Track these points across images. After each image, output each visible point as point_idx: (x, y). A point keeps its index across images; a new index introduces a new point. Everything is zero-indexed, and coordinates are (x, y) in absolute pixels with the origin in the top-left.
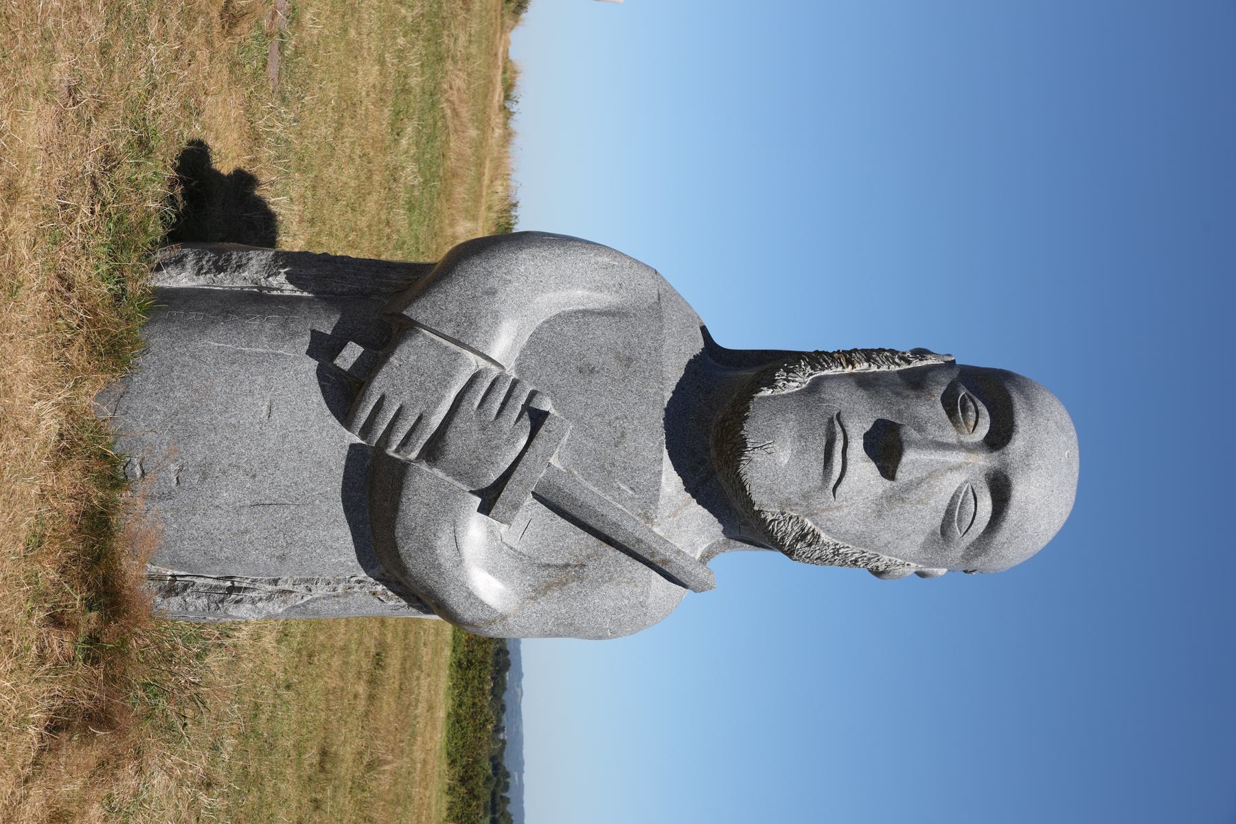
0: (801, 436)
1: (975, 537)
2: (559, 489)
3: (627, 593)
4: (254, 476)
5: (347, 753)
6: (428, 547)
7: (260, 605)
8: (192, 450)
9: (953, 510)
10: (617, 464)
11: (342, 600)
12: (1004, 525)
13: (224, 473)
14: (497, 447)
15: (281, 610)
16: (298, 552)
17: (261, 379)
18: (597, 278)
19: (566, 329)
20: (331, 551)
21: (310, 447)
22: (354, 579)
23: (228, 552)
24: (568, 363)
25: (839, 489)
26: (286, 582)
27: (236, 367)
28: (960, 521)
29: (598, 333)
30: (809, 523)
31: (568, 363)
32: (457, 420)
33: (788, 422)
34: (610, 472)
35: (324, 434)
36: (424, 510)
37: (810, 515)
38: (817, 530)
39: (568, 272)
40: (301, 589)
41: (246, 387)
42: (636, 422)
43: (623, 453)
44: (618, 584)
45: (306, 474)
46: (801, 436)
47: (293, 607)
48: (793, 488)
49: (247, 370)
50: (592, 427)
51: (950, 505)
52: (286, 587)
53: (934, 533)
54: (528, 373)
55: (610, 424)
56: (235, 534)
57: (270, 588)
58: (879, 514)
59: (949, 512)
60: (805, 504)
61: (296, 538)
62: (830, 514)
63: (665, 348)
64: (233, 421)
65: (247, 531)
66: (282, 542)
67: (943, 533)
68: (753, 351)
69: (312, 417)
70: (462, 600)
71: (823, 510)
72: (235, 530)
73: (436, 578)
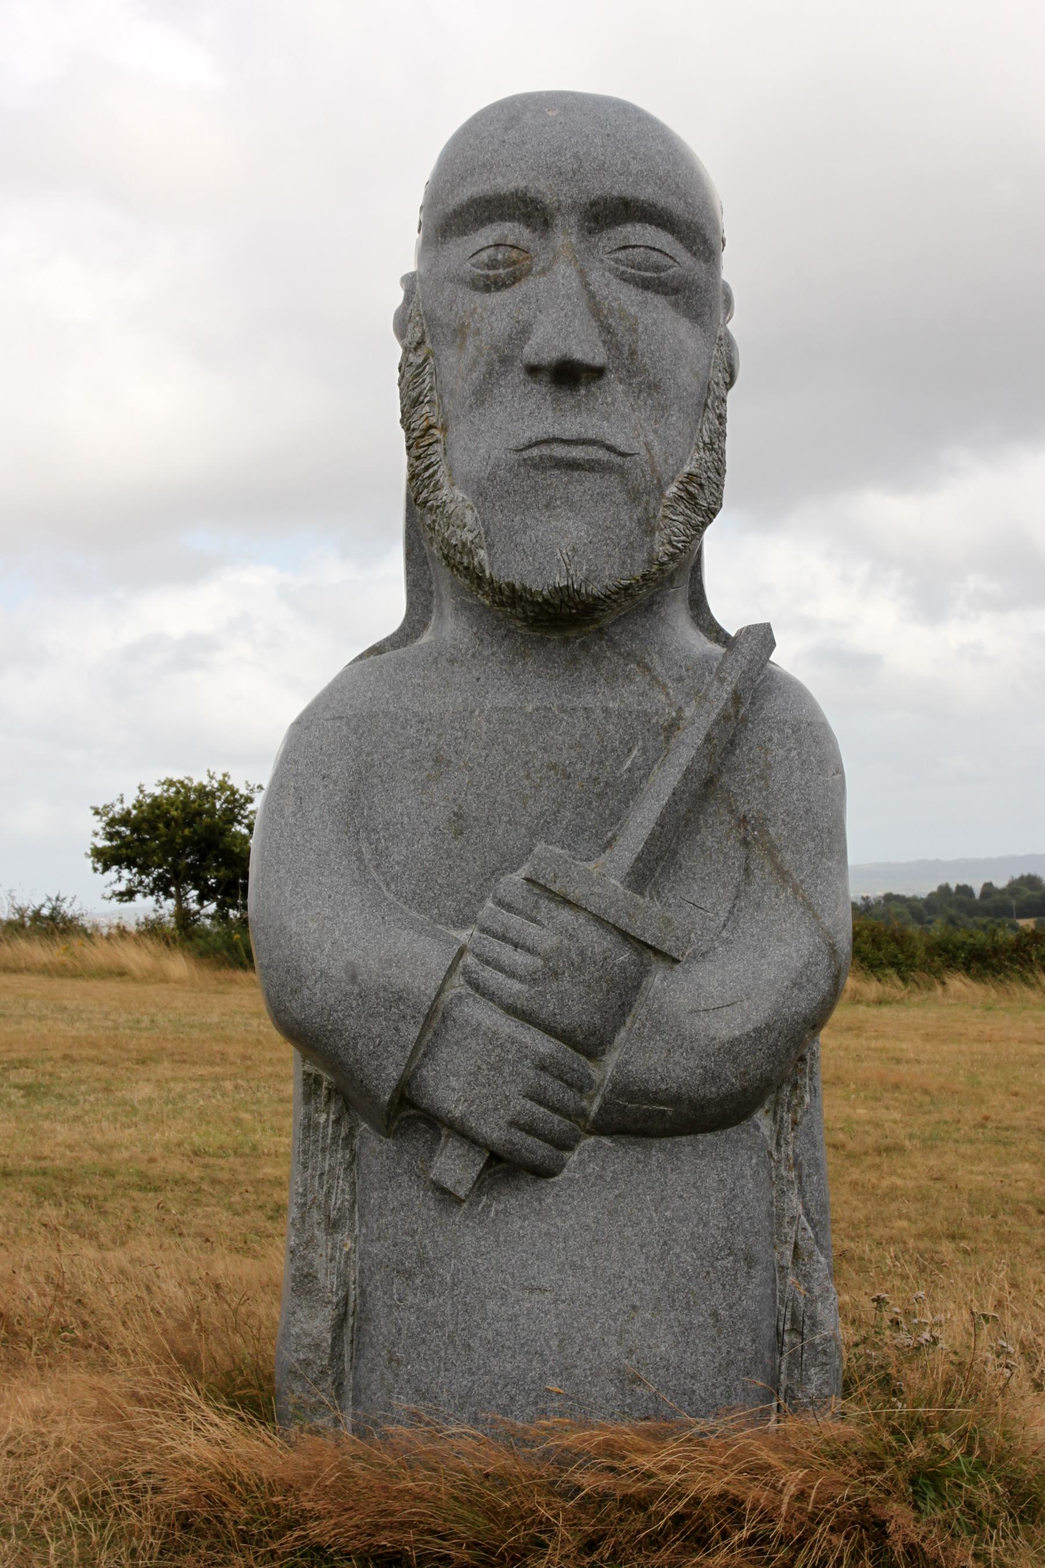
0: (547, 506)
1: (679, 246)
2: (639, 859)
3: (781, 752)
4: (634, 1307)
5: (269, 1070)
6: (730, 1049)
7: (817, 1291)
8: (600, 1401)
9: (644, 280)
10: (595, 774)
11: (806, 1171)
12: (661, 203)
13: (631, 1352)
14: (582, 953)
15: (822, 1259)
16: (741, 1238)
17: (491, 1305)
18: (317, 812)
19: (397, 857)
20: (738, 1191)
21: (587, 1228)
22: (775, 1153)
23: (745, 1341)
24: (448, 852)
25: (623, 448)
26: (782, 1254)
27: (475, 1343)
28: (657, 268)
29: (399, 808)
30: (672, 490)
31: (448, 852)
32: (544, 1014)
33: (527, 526)
34: (607, 783)
35: (568, 1208)
36: (677, 1057)
37: (661, 488)
38: (681, 477)
39: (312, 856)
40: (790, 1231)
41: (504, 1327)
42: (532, 749)
43: (579, 766)
44: (769, 766)
45: (628, 1232)
46: (547, 506)
47: (817, 1242)
48: (624, 516)
49: (478, 1326)
50: (543, 814)
51: (636, 284)
52: (789, 1254)
53: (675, 305)
54: (467, 910)
55: (537, 787)
56: (720, 1332)
57: (791, 1279)
58: (654, 387)
59: (646, 285)
60: (645, 498)
61: (722, 1242)
62: (659, 459)
63: (417, 708)
64: (554, 1343)
65: (715, 1314)
66: (728, 1262)
67: (676, 291)
68: (408, 573)
69: (544, 1228)
70: (804, 995)
71: (654, 471)
72: (714, 1332)
73: (775, 1034)
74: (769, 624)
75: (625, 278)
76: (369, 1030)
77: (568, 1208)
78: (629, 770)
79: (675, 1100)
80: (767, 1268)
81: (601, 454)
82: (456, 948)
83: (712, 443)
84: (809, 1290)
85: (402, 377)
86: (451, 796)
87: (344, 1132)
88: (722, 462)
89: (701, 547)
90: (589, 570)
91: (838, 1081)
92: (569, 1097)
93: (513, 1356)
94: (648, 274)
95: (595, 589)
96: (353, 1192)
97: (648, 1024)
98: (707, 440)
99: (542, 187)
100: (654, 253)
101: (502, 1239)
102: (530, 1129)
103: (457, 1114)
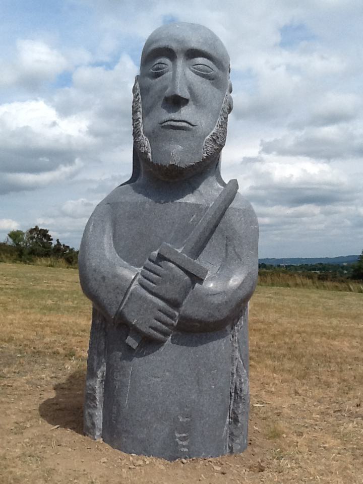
1: (214, 66)
3: (239, 218)
6: (218, 307)
7: (242, 380)
17: (142, 381)
18: (99, 231)
21: (173, 359)
25: (193, 124)
28: (207, 72)
35: (167, 353)
53: (212, 84)
59: (203, 76)
67: (213, 79)
69: (160, 358)
74: (236, 180)
75: (196, 73)
76: (108, 297)
77: (167, 353)
78: (192, 222)
79: (200, 322)
80: (227, 373)
81: (184, 124)
82: (136, 273)
83: (222, 125)
84: (240, 380)
85: (303, 259)
86: (138, 227)
87: (103, 326)
88: (226, 137)
89: (219, 157)
90: (180, 160)
91: (263, 113)
92: (168, 320)
93: (148, 397)
94: (204, 73)
95: (183, 166)
96: (105, 344)
97: (193, 299)
98: (220, 124)
99: (174, 46)
100: (206, 67)
101: (147, 361)
102: (155, 329)
103: (133, 323)
